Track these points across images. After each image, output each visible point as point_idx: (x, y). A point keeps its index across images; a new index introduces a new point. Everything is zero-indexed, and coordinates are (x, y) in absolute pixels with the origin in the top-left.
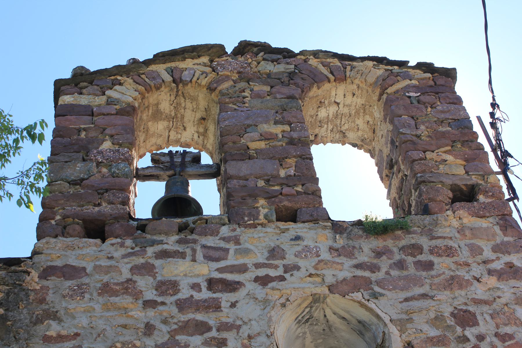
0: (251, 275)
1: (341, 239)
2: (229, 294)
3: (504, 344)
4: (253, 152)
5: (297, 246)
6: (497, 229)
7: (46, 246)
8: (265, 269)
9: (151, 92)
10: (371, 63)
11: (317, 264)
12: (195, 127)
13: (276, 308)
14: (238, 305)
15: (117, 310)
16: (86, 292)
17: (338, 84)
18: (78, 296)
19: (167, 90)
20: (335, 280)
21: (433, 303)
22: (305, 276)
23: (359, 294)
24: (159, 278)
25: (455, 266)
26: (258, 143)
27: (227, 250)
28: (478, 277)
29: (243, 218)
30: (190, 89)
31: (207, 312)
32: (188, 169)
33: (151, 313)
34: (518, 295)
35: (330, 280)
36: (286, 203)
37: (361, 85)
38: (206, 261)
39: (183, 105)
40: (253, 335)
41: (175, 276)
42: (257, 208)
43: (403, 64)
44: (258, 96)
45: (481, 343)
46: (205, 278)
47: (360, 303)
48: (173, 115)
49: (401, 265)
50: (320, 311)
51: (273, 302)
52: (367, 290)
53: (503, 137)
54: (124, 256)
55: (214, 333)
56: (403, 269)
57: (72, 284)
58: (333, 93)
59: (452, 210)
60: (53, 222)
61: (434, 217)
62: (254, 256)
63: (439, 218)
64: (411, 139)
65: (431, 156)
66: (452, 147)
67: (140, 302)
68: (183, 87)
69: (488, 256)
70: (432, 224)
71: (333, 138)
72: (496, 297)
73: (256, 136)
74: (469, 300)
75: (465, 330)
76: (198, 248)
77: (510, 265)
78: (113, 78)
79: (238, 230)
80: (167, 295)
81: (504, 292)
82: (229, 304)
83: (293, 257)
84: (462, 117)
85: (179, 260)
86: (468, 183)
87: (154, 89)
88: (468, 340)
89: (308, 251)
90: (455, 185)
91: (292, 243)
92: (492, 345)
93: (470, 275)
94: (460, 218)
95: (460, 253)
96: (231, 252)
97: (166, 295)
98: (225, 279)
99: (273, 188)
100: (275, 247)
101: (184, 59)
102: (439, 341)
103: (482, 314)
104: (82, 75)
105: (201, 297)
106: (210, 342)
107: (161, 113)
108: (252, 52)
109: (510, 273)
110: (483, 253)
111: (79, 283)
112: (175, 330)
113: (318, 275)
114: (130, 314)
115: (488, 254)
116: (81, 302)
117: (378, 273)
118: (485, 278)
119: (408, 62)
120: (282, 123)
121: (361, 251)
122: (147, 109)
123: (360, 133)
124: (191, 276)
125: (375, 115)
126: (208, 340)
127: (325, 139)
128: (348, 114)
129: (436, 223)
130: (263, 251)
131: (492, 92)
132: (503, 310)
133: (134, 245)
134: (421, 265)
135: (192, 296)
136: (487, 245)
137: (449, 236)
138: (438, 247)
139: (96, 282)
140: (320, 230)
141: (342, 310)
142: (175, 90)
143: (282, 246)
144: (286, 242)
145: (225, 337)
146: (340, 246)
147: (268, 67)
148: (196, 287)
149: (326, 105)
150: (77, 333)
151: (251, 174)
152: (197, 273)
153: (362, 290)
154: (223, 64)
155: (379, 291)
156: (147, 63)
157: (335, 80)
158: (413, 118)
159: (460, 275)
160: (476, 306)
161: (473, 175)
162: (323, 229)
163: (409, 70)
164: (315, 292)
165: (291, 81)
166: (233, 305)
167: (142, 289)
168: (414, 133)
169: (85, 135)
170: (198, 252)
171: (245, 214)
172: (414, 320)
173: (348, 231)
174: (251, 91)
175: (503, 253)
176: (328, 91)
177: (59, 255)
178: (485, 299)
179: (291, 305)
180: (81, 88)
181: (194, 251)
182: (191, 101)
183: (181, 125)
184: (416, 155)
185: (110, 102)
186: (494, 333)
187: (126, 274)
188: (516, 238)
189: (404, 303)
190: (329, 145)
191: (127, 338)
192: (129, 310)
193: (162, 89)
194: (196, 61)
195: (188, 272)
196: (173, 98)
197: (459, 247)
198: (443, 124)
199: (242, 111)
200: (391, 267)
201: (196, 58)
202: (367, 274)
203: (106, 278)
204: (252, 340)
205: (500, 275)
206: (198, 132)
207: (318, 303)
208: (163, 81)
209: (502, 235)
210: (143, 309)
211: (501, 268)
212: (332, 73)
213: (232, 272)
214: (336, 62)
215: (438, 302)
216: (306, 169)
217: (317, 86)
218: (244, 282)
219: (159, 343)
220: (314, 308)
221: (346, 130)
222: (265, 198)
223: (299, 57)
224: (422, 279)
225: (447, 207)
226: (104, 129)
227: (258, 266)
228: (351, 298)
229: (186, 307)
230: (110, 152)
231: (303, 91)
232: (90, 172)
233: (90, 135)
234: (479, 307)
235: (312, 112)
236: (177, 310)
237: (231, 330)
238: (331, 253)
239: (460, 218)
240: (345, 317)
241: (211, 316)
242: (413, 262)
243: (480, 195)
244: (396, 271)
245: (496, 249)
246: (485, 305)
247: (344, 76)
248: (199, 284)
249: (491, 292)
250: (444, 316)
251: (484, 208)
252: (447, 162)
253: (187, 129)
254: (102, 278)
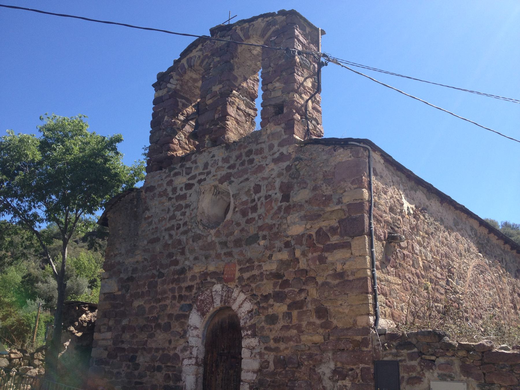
101: (191, 51)
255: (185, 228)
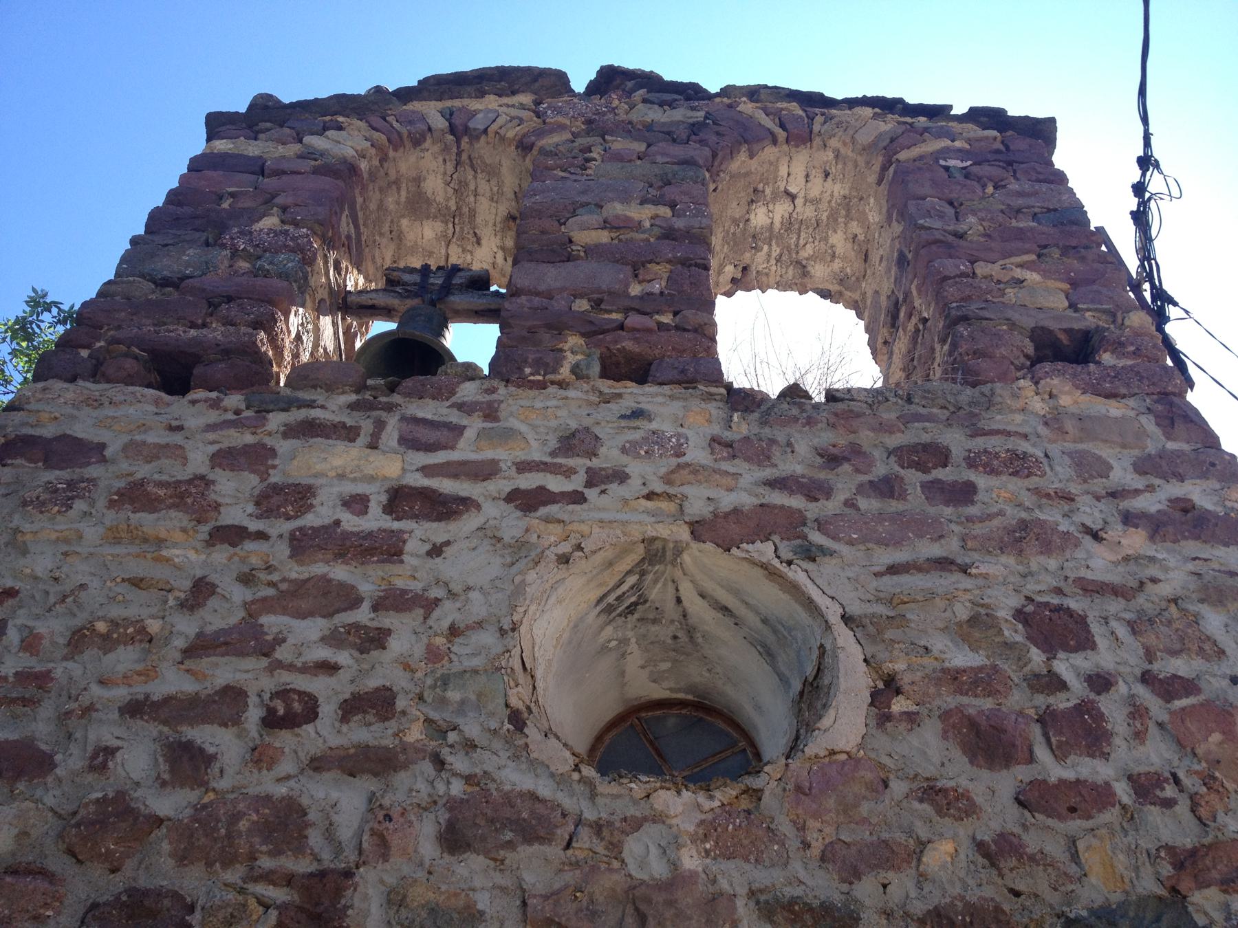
0: (503, 485)
1: (743, 423)
2: (435, 525)
3: (1168, 706)
4: (579, 248)
5: (633, 431)
6: (1148, 423)
7: (39, 396)
8: (541, 475)
9: (402, 148)
10: (868, 112)
11: (672, 472)
12: (498, 237)
13: (543, 564)
14: (448, 551)
15: (137, 542)
16: (83, 497)
17: (793, 150)
18: (56, 505)
19: (436, 148)
20: (711, 509)
21: (967, 583)
22: (637, 495)
23: (768, 548)
24: (275, 478)
25: (1034, 498)
26: (593, 233)
27: (459, 430)
28: (1095, 527)
29: (520, 369)
30: (483, 149)
31: (363, 564)
32: (452, 298)
33: (221, 554)
34: (1207, 578)
35: (697, 507)
36: (628, 345)
37: (843, 151)
38: (402, 449)
39: (472, 187)
40: (462, 626)
41: (315, 476)
42: (561, 350)
43: (938, 112)
44: (618, 158)
45: (1102, 698)
46: (387, 485)
47: (766, 569)
48: (454, 208)
49: (887, 488)
50: (665, 585)
51: (539, 550)
52: (788, 539)
53: (1161, 249)
54: (211, 428)
55: (363, 615)
56: (892, 497)
57: (56, 479)
58: (783, 171)
59: (1032, 378)
60: (84, 353)
61: (986, 389)
62: (523, 446)
63: (998, 391)
64: (942, 238)
65: (988, 270)
66: (1039, 256)
67: (205, 529)
68: (471, 143)
69: (1123, 481)
70: (976, 404)
71: (781, 276)
72: (1145, 580)
73: (594, 222)
74: (1070, 581)
75: (1054, 658)
76: (392, 422)
77: (1184, 507)
78: (328, 118)
79: (502, 391)
80: (278, 516)
81: (1166, 570)
82: (428, 547)
83: (615, 453)
84: (1066, 205)
85: (338, 442)
86: (1076, 326)
87: (408, 143)
88: (1062, 686)
89: (656, 443)
90: (1043, 328)
91: (623, 425)
92: (1134, 705)
93: (1073, 523)
94: (1051, 396)
95: (1047, 469)
96: (470, 434)
97: (276, 518)
98: (434, 491)
99: (606, 316)
100: (577, 431)
101: (481, 94)
102: (976, 683)
103: (1106, 620)
104: (266, 107)
105: (359, 526)
106: (344, 636)
107: (428, 202)
108: (624, 90)
109: (1183, 523)
110: (1111, 475)
111: (75, 477)
112: (264, 600)
113: (669, 497)
114: (164, 553)
115: (1122, 474)
116: (59, 517)
117: (825, 502)
118: (1115, 531)
119: (951, 107)
120: (656, 202)
121: (789, 450)
122: (394, 187)
123: (837, 265)
124: (354, 480)
125: (870, 218)
126: (342, 630)
127: (764, 279)
128: (813, 221)
129: (990, 403)
130: (547, 438)
131: (1145, 120)
132: (1166, 614)
133: (243, 406)
134: (942, 490)
135: (337, 523)
136: (1120, 456)
137: (1020, 430)
138: (990, 453)
139: (117, 477)
140: (698, 401)
141: (722, 586)
142: (455, 150)
143: (597, 431)
144: (608, 422)
145: (386, 627)
146: (737, 437)
147: (655, 115)
148: (357, 503)
149: (768, 198)
150: (12, 588)
151: (562, 289)
152: (371, 472)
153: (776, 538)
154: (560, 107)
155: (820, 543)
156: (405, 95)
157: (787, 141)
158: (951, 203)
159: (1045, 521)
160: (1089, 599)
161: (1088, 310)
162: (704, 400)
163: (951, 124)
164: (654, 534)
165: (693, 137)
166: (436, 551)
167: (220, 500)
168: (951, 228)
169: (230, 205)
170: (389, 428)
171: (526, 361)
172: (909, 621)
173: (763, 408)
174: (605, 150)
175: (1165, 478)
176: (771, 163)
177: (57, 415)
178: (1115, 583)
179: (584, 561)
180: (258, 132)
181: (380, 425)
182: (487, 178)
183: (472, 232)
184: (949, 266)
185: (309, 154)
186: (1138, 672)
187: (198, 460)
188: (1199, 446)
189: (886, 579)
190: (772, 293)
191: (132, 612)
192: (168, 544)
193: (427, 144)
194: (505, 100)
195: (348, 471)
196: (450, 167)
197: (1046, 456)
198: (1021, 216)
199: (575, 181)
200: (860, 489)
201: (507, 96)
202: (796, 502)
203: (143, 471)
204: (457, 640)
205: (1156, 526)
206: (503, 248)
207: (660, 564)
208: (430, 129)
209: (1163, 438)
210: (204, 544)
211: (1159, 511)
212: (782, 126)
213: (455, 476)
214: (795, 108)
215: (981, 582)
216: (691, 283)
217: (749, 149)
218: (481, 500)
219: (209, 629)
220: (650, 577)
221: (807, 259)
222: (583, 335)
223: (718, 100)
224: (941, 522)
225: (1019, 374)
226: (273, 197)
227: (523, 467)
228: (744, 555)
229: (311, 546)
230: (268, 234)
231: (714, 156)
232: (210, 265)
233: (240, 205)
234: (1097, 601)
235: (735, 210)
236: (287, 552)
237: (409, 609)
238: (712, 449)
239: (1051, 396)
240: (729, 607)
241: (371, 572)
242: (921, 482)
243: (1105, 352)
244: (873, 502)
245: (1141, 467)
246: (1113, 597)
247: (807, 131)
248: (367, 496)
249: (1132, 567)
250: (997, 618)
251: (1115, 377)
252: (1024, 284)
253: (483, 242)
254: (133, 469)
255: (362, 733)
